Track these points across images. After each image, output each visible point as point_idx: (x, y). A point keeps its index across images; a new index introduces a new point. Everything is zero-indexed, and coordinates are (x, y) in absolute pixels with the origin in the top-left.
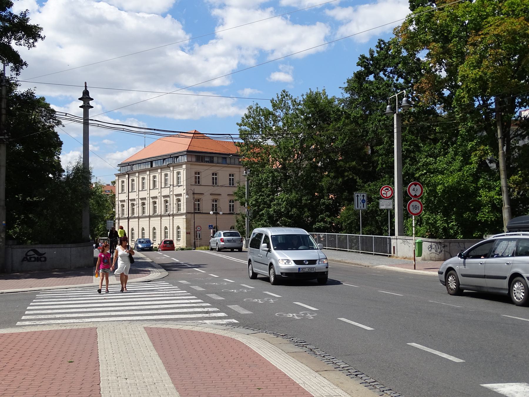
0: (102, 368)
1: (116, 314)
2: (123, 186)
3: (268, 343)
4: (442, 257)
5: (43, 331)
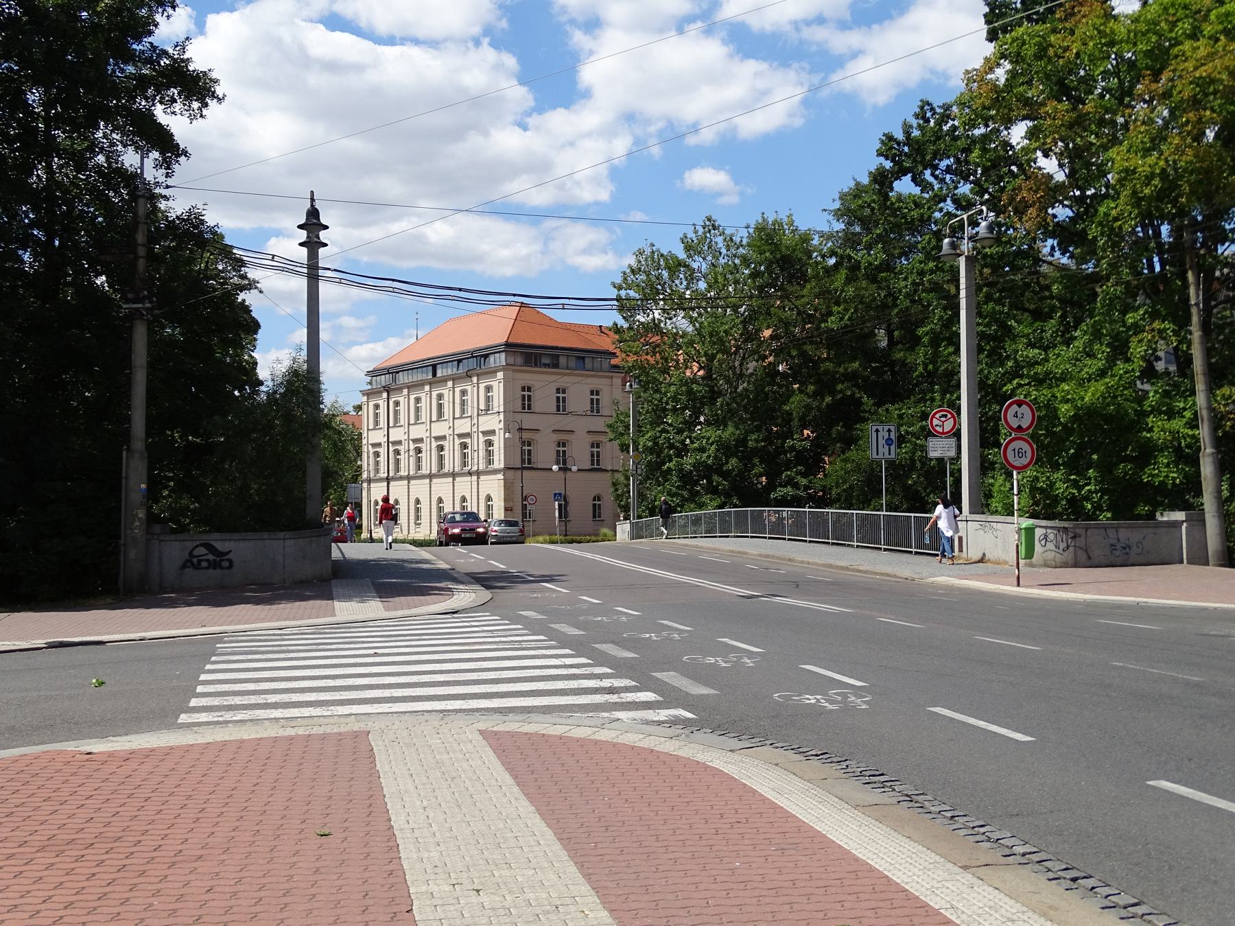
0: (407, 854)
1: (405, 694)
2: (376, 416)
3: (791, 776)
4: (1069, 558)
5: (243, 741)
